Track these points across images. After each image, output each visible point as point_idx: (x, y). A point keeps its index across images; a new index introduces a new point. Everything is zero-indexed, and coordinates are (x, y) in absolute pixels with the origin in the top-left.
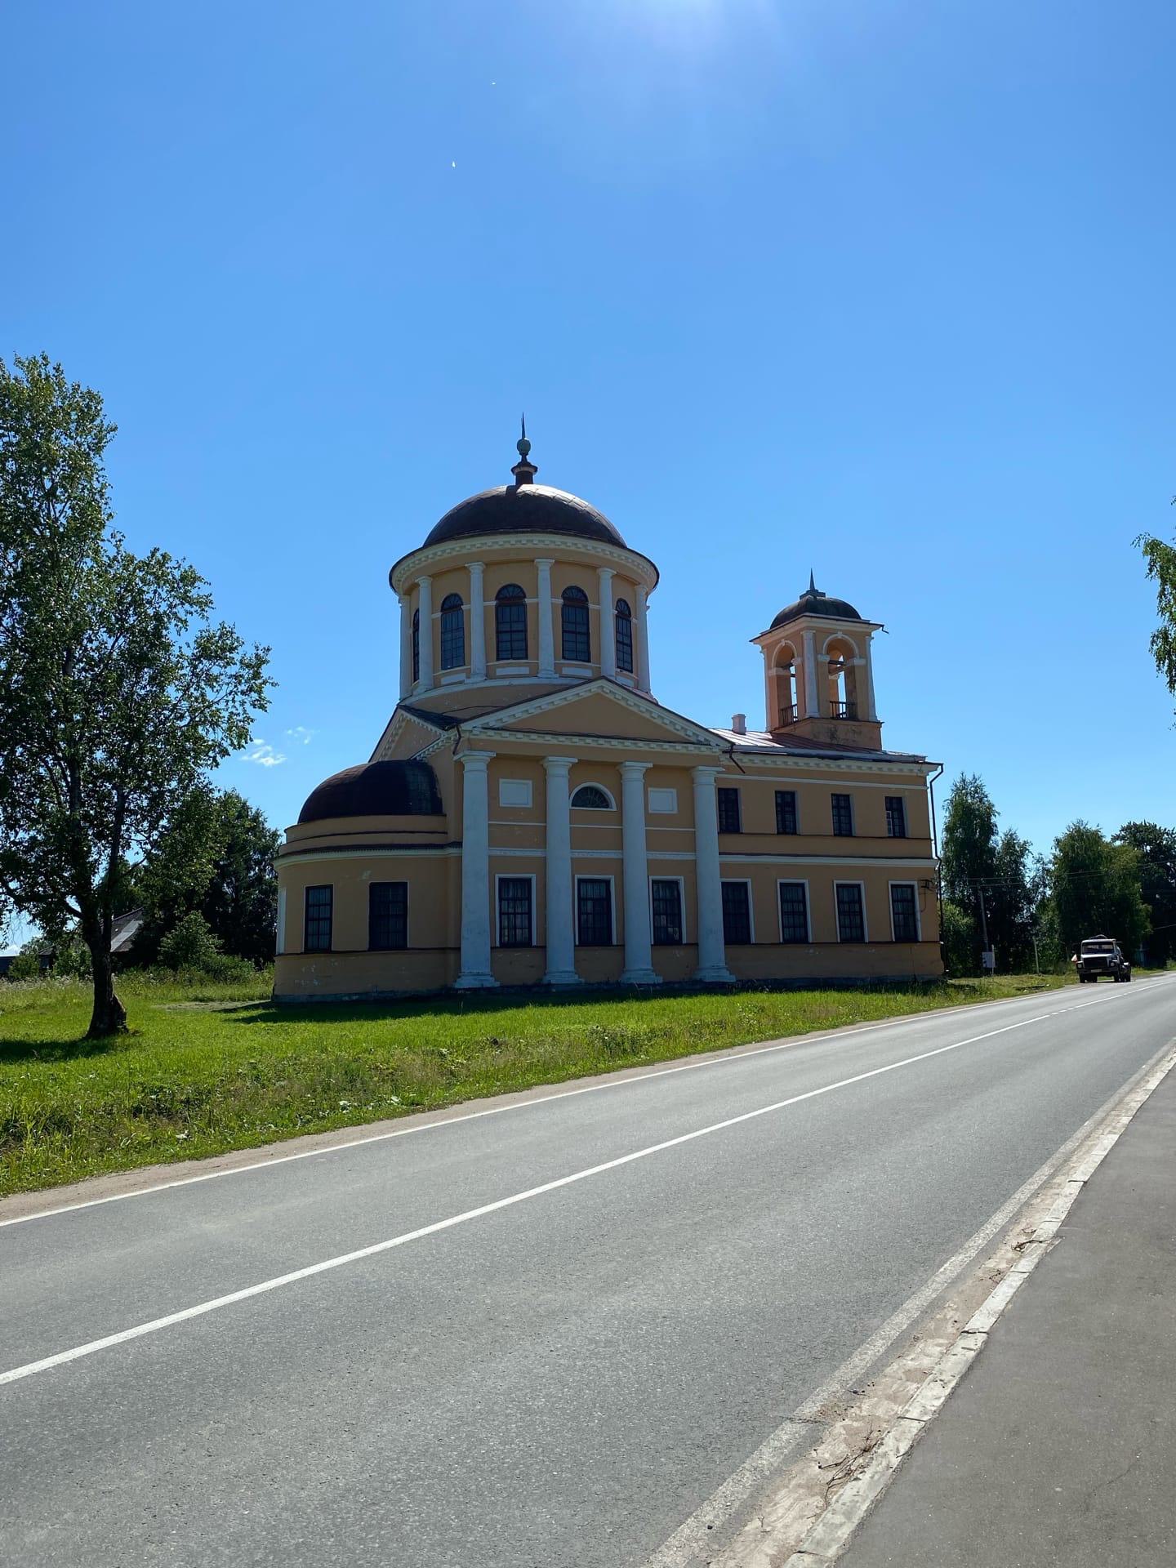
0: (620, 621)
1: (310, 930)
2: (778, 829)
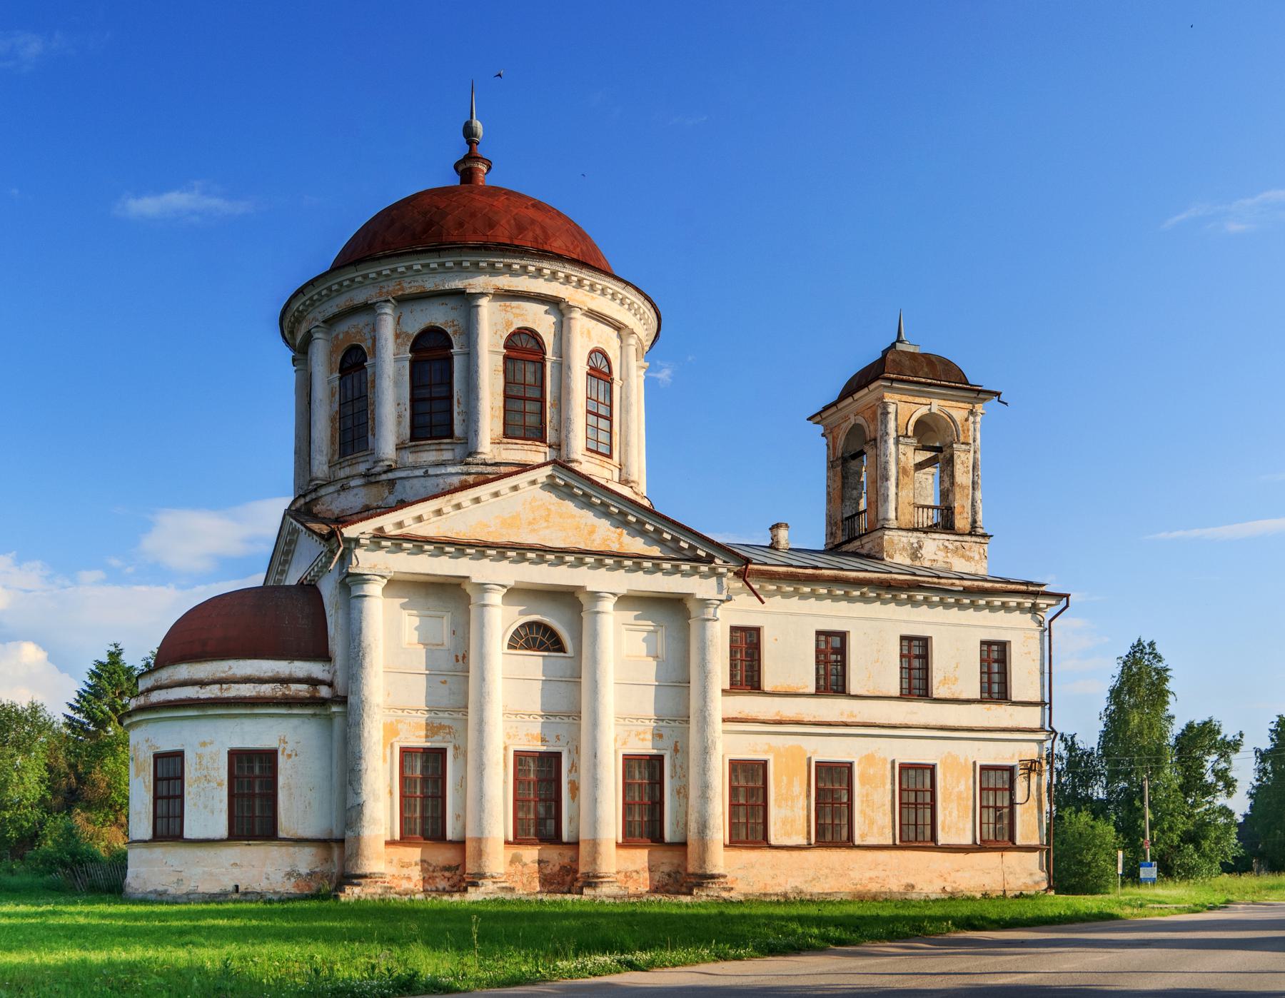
0: (595, 381)
1: (159, 811)
2: (901, 688)
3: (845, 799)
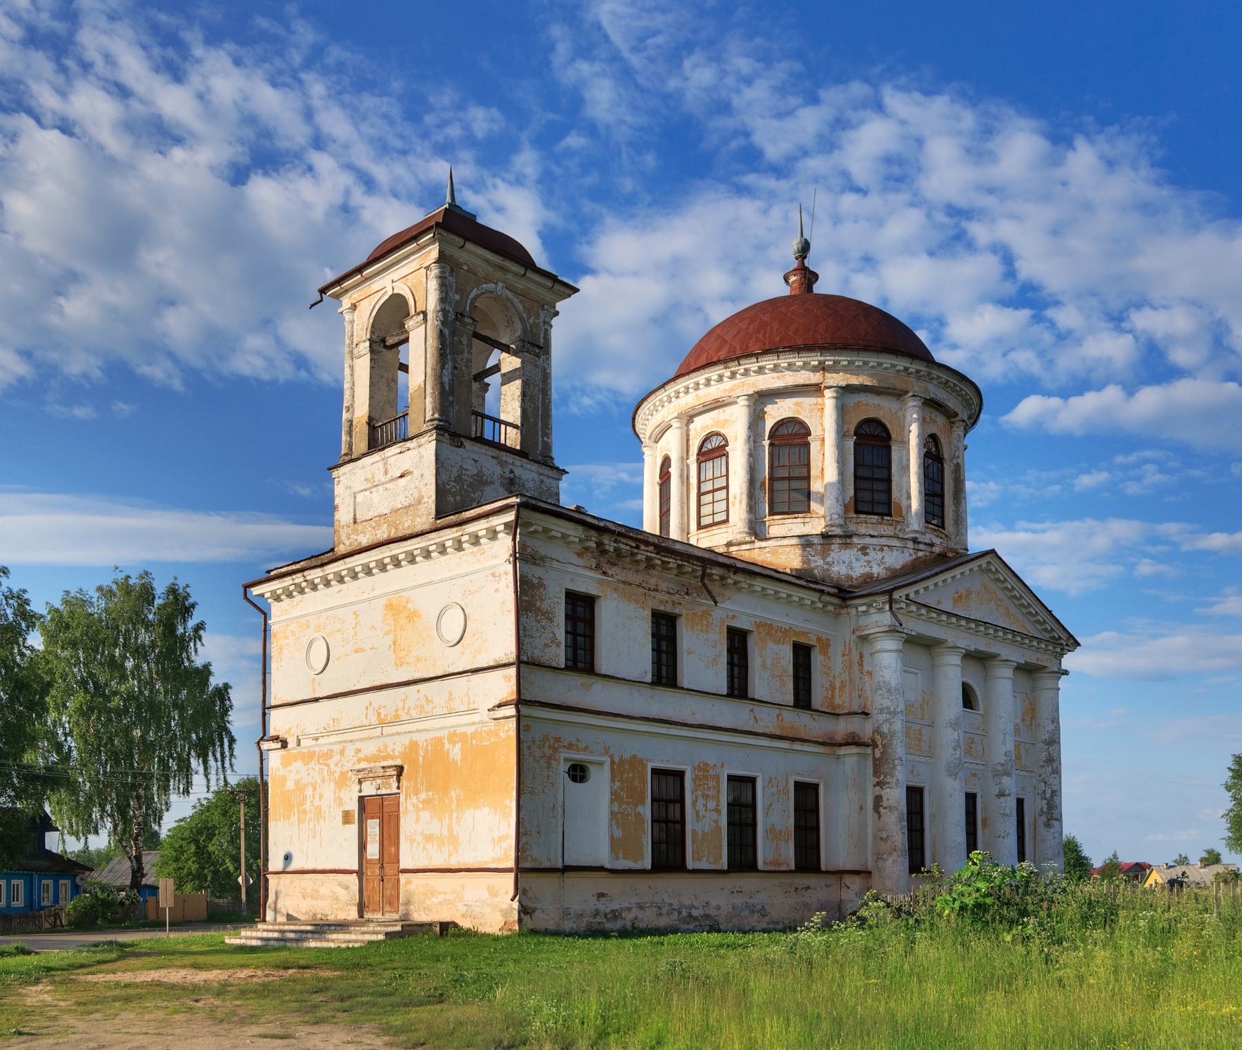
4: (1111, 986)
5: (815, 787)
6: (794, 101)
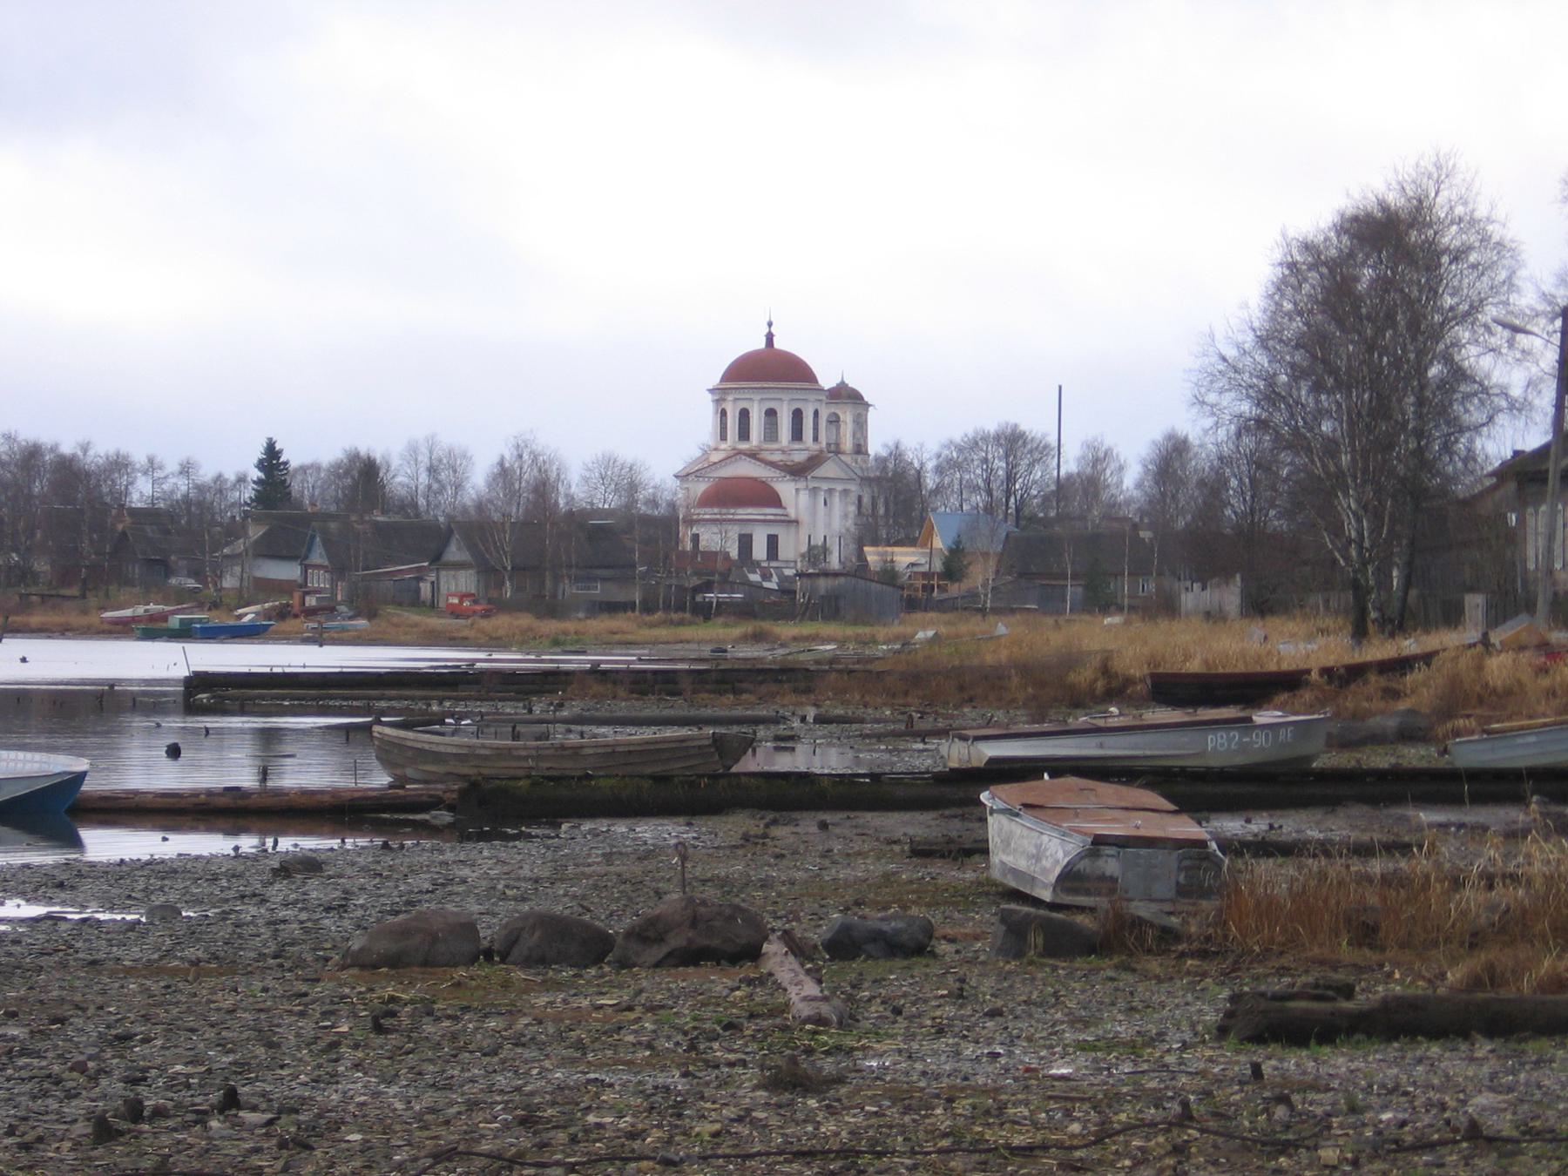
3: (99, 729)
4: (498, 1099)
5: (777, 536)
6: (716, 538)
